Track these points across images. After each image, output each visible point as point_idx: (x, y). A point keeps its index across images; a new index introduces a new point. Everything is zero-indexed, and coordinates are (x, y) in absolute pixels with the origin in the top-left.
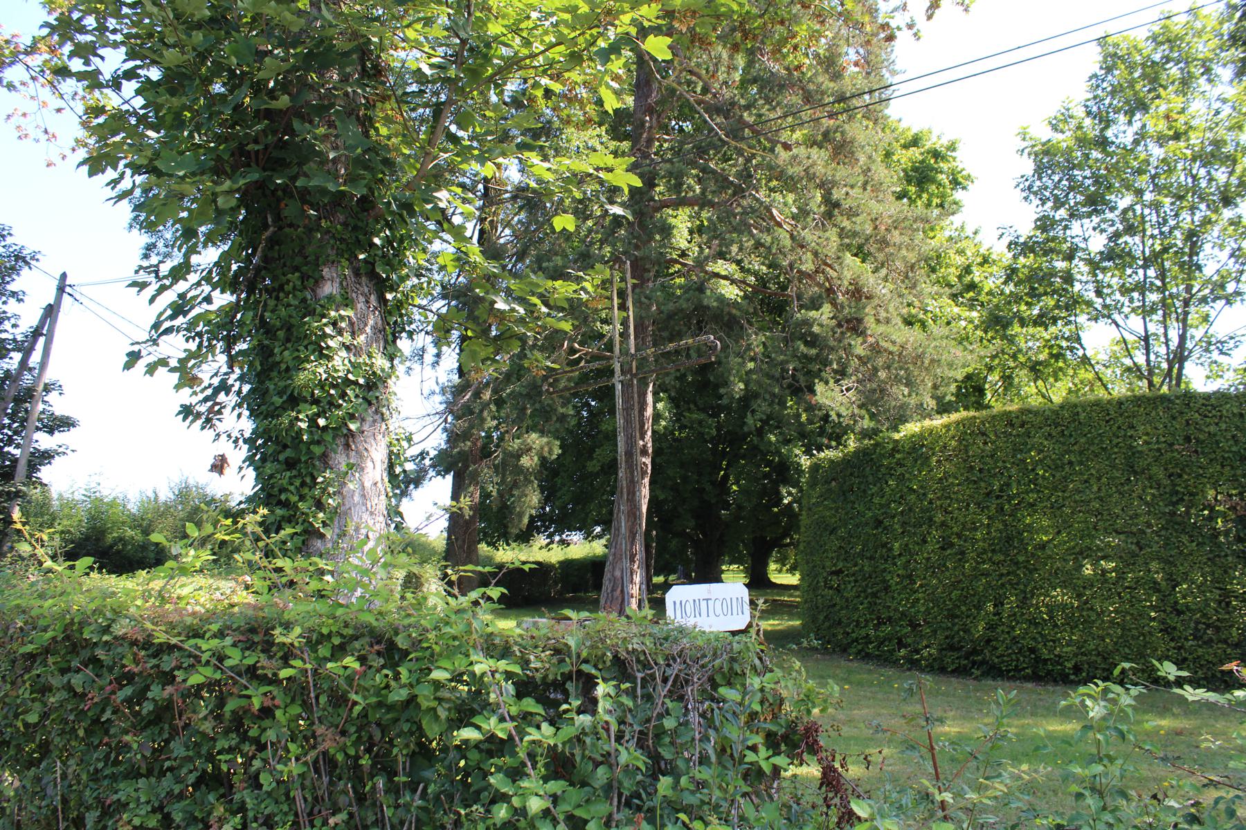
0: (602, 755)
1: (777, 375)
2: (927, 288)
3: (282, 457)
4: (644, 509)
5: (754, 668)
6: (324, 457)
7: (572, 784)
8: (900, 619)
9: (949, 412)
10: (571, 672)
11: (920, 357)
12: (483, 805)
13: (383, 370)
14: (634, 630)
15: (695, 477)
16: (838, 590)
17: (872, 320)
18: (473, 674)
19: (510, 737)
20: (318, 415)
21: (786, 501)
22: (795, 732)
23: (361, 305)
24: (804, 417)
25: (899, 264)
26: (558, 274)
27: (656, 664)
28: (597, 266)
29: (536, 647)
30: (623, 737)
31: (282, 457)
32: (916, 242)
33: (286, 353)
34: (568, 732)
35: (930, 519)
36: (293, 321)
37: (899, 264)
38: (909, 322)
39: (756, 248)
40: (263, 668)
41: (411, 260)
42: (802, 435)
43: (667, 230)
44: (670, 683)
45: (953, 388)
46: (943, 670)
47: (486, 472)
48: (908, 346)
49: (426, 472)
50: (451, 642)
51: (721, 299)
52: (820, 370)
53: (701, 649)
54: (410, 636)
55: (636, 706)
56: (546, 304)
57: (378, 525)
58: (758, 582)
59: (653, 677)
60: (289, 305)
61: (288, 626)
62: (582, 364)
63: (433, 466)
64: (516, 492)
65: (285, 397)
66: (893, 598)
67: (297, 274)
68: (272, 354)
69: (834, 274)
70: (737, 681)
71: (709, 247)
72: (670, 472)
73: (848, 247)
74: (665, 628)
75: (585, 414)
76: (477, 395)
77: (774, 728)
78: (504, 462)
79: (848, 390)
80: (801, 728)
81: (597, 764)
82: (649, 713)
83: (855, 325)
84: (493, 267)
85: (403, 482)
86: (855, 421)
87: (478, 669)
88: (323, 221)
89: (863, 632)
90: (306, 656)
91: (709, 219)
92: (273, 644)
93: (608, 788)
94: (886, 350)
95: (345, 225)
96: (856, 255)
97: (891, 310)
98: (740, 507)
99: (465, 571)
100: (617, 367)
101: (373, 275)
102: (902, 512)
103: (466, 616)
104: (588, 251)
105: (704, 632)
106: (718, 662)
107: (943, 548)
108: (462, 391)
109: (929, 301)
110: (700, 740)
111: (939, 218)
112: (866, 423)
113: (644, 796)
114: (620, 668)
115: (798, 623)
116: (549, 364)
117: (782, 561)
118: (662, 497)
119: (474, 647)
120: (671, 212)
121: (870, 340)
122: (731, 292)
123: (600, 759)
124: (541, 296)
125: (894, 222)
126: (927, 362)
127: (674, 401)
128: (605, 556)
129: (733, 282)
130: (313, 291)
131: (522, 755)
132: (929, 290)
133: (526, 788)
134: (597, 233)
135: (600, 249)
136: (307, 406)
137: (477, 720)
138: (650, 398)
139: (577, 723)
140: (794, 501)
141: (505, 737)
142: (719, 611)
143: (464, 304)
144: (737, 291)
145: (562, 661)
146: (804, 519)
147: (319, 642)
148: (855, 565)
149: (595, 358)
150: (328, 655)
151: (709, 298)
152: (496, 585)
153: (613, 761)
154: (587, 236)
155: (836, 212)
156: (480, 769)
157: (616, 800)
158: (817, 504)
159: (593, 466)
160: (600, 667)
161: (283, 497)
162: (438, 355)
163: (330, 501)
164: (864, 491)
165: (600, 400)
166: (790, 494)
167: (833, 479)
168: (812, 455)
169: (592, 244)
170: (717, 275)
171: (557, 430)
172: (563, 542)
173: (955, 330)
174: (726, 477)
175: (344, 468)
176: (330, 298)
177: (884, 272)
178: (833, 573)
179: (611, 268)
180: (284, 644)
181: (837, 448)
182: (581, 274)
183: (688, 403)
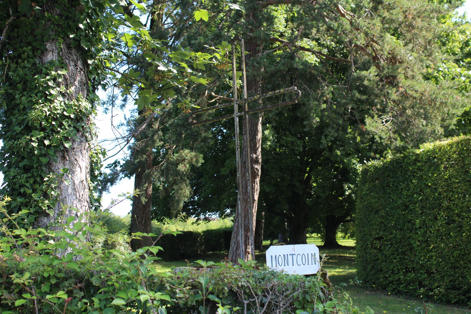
2: (438, 55)
3: (21, 165)
5: (319, 298)
6: (49, 165)
8: (420, 269)
9: (452, 136)
10: (202, 300)
11: (433, 100)
13: (86, 109)
14: (243, 273)
16: (380, 250)
17: (403, 76)
18: (140, 301)
20: (45, 138)
21: (347, 193)
23: (71, 68)
24: (359, 139)
25: (421, 40)
27: (256, 295)
28: (224, 43)
29: (180, 284)
31: (21, 165)
32: (432, 26)
33: (24, 98)
35: (440, 205)
36: (27, 78)
37: (421, 40)
38: (427, 78)
39: (328, 31)
40: (6, 299)
41: (103, 38)
42: (358, 151)
43: (271, 20)
44: (265, 307)
45: (455, 121)
46: (448, 302)
48: (426, 94)
50: (126, 281)
51: (306, 64)
52: (369, 109)
53: (285, 285)
54: (100, 277)
56: (191, 67)
57: (84, 208)
58: (329, 244)
59: (254, 303)
60: (25, 67)
61: (21, 272)
62: (217, 105)
63: (122, 171)
64: (175, 187)
65: (23, 127)
66: (416, 255)
67: (29, 47)
68: (14, 99)
69: (378, 47)
71: (298, 31)
73: (387, 30)
75: (219, 138)
76: (150, 125)
79: (387, 122)
83: (391, 81)
84: (157, 44)
85: (102, 182)
86: (391, 142)
87: (143, 298)
88: (46, 13)
89: (396, 277)
90: (33, 292)
91: (298, 12)
92: (12, 284)
94: (411, 96)
95: (61, 15)
96: (393, 35)
97: (415, 70)
98: (318, 197)
99: (135, 236)
100: (236, 107)
101: (79, 48)
102: (421, 200)
103: (135, 265)
104: (220, 33)
105: (288, 275)
106: (295, 294)
107: (448, 224)
109: (440, 64)
111: (448, 10)
112: (399, 143)
115: (354, 271)
116: (193, 105)
117: (345, 231)
118: (268, 190)
119: (141, 284)
120: (274, 8)
121: (401, 90)
122: (312, 59)
124: (187, 62)
125: (418, 13)
126: (438, 104)
127: (276, 129)
128: (232, 228)
129: (313, 53)
130: (40, 58)
132: (441, 57)
134: (226, 21)
136: (37, 132)
138: (260, 127)
140: (353, 193)
143: (142, 68)
146: (358, 205)
147: (42, 282)
148: (391, 234)
149: (224, 101)
150: (48, 290)
154: (220, 24)
155: (380, 7)
158: (367, 195)
159: (224, 171)
160: (221, 296)
161: (22, 190)
162: (125, 100)
163: (53, 193)
164: (397, 187)
166: (349, 188)
167: (377, 179)
169: (222, 29)
170: (303, 49)
171: (202, 147)
172: (207, 220)
173: (457, 83)
175: (61, 171)
176: (52, 63)
177: (411, 45)
178: (377, 239)
180: (19, 284)
181: (379, 159)
182: (213, 48)
183: (285, 130)
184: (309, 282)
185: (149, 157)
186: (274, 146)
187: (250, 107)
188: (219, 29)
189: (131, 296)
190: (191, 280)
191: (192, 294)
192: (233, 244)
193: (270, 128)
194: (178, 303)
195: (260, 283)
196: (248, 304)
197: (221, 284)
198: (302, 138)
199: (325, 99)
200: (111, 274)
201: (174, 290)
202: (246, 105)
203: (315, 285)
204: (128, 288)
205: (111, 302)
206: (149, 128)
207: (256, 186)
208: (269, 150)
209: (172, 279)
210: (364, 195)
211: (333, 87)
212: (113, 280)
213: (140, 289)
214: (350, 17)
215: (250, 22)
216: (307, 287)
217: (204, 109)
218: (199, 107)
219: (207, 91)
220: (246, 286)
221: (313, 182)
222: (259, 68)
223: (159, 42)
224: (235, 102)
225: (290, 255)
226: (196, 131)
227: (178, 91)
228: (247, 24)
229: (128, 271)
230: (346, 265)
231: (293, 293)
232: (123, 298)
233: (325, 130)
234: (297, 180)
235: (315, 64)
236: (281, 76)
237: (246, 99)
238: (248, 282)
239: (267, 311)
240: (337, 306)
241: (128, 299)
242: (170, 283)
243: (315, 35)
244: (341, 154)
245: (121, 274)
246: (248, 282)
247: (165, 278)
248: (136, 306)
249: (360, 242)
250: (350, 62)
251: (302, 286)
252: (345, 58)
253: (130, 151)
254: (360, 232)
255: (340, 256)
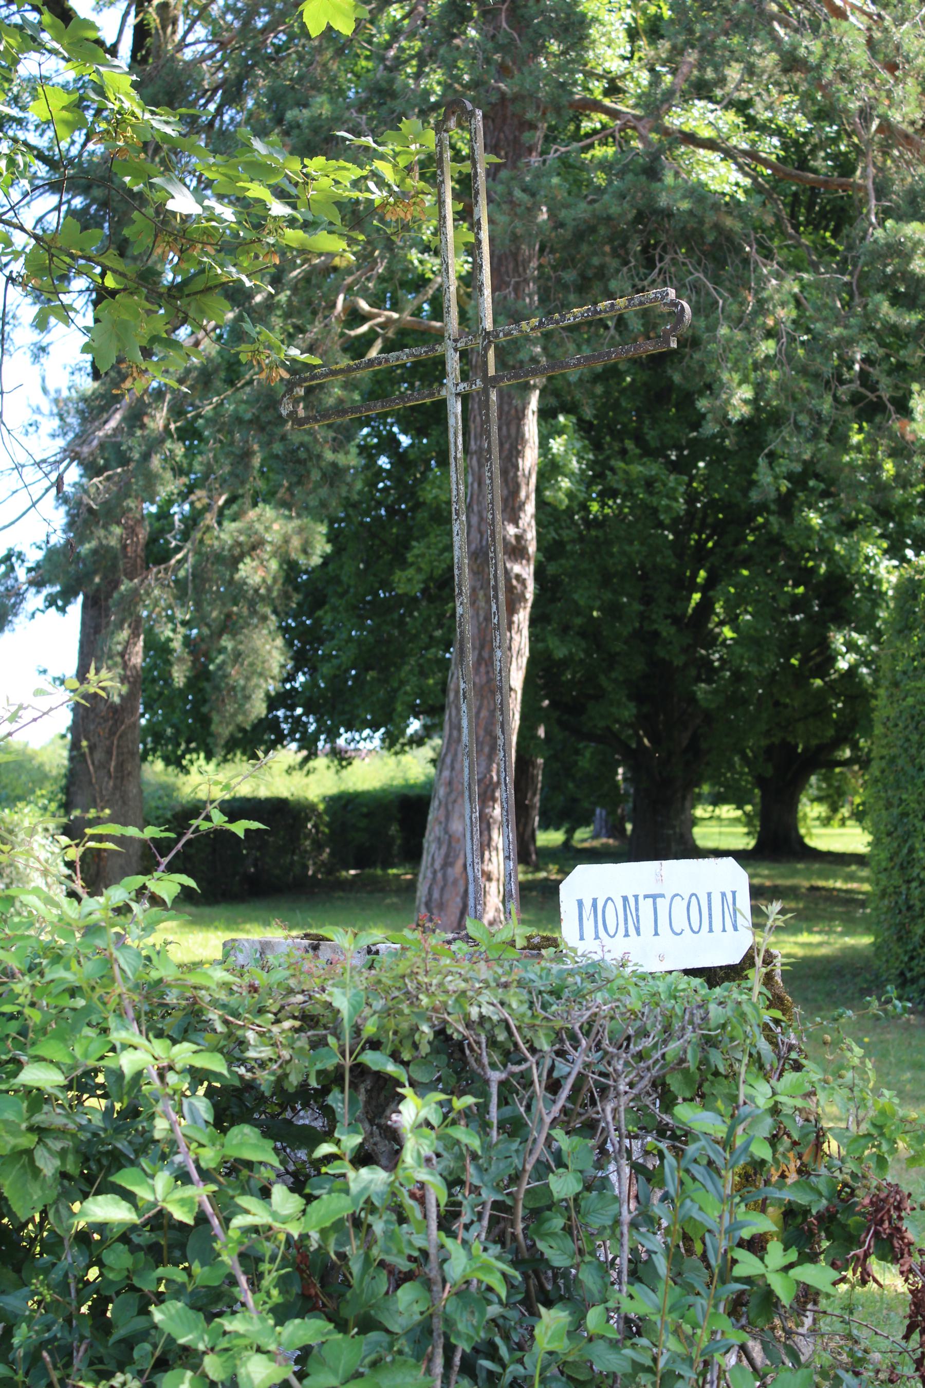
0: (410, 1258)
1: (827, 372)
4: (517, 678)
5: (757, 1061)
7: (342, 1326)
10: (339, 1068)
12: (140, 1374)
14: (484, 971)
15: (637, 607)
18: (119, 1075)
19: (202, 1219)
21: (842, 665)
22: (850, 1208)
24: (889, 468)
26: (317, 142)
27: (533, 1050)
29: (261, 1011)
30: (457, 1215)
34: (332, 1206)
44: (565, 1092)
47: (156, 595)
49: (20, 596)
51: (698, 193)
55: (488, 1147)
58: (776, 844)
62: (373, 353)
70: (722, 1088)
71: (673, 72)
72: (580, 597)
74: (555, 968)
76: (136, 417)
77: (802, 1199)
78: (198, 575)
80: (863, 1199)
81: (400, 1279)
82: (517, 1161)
84: (165, 125)
87: (128, 1062)
93: (423, 1333)
99: (100, 838)
100: (453, 363)
106: (673, 1047)
108: (103, 409)
110: (634, 1225)
113: (503, 1351)
114: (453, 1060)
115: (866, 940)
116: (294, 352)
117: (833, 799)
118: (560, 652)
119: (120, 1013)
122: (722, 177)
123: (404, 1265)
128: (430, 785)
129: (729, 154)
131: (228, 1258)
133: (238, 1335)
134: (411, 35)
135: (418, 75)
137: (124, 1178)
138: (531, 427)
139: (354, 1187)
141: (189, 1220)
142: (680, 922)
143: (104, 204)
144: (735, 176)
145: (318, 1044)
146: (882, 707)
151: (668, 189)
152: (171, 868)
153: (434, 1274)
154: (388, 46)
156: (133, 1288)
157: (439, 1361)
159: (407, 582)
160: (406, 1057)
165: (418, 432)
166: (851, 646)
168: (904, 559)
169: (399, 63)
170: (691, 139)
171: (323, 504)
174: (706, 607)
179: (440, 128)
184: (721, 1003)
185: (131, 531)
186: (582, 496)
187: (501, 362)
188: (386, 68)
189: (86, 1055)
190: (300, 998)
191: (302, 1048)
192: (434, 846)
193: (570, 430)
194: (254, 1080)
195: (544, 1007)
196: (502, 1083)
197: (407, 1011)
198: (682, 467)
199: (770, 322)
200: (13, 976)
201: (239, 1033)
202: (491, 353)
203: (743, 1015)
204: (74, 1029)
205: (15, 1075)
206: (132, 427)
207: (516, 637)
208: (568, 507)
209: (231, 992)
210: (905, 673)
211: (801, 280)
212: (21, 1000)
213: (117, 1030)
214: (865, 19)
215: (501, 39)
216: (712, 1024)
217: (338, 367)
218: (317, 361)
219: (341, 297)
220: (495, 1018)
221: (721, 623)
222: (532, 211)
223: (172, 119)
224: (450, 343)
225: (646, 897)
226: (302, 444)
227: (237, 295)
228: (490, 45)
229: (74, 965)
230: (832, 919)
231: (665, 1042)
232: (58, 1065)
233: (770, 434)
234: (666, 617)
235: (732, 197)
236: (611, 240)
237: (488, 333)
238: (502, 1004)
239: (569, 1105)
240: (819, 1092)
241: (73, 1068)
242: (224, 1006)
243: (737, 89)
244: (825, 522)
245: (48, 977)
246: (502, 1004)
247: (207, 989)
248: (101, 1086)
249: (886, 840)
250: (861, 188)
251: (697, 1020)
252: (841, 175)
253: (63, 509)
254: (889, 805)
255: (813, 889)
